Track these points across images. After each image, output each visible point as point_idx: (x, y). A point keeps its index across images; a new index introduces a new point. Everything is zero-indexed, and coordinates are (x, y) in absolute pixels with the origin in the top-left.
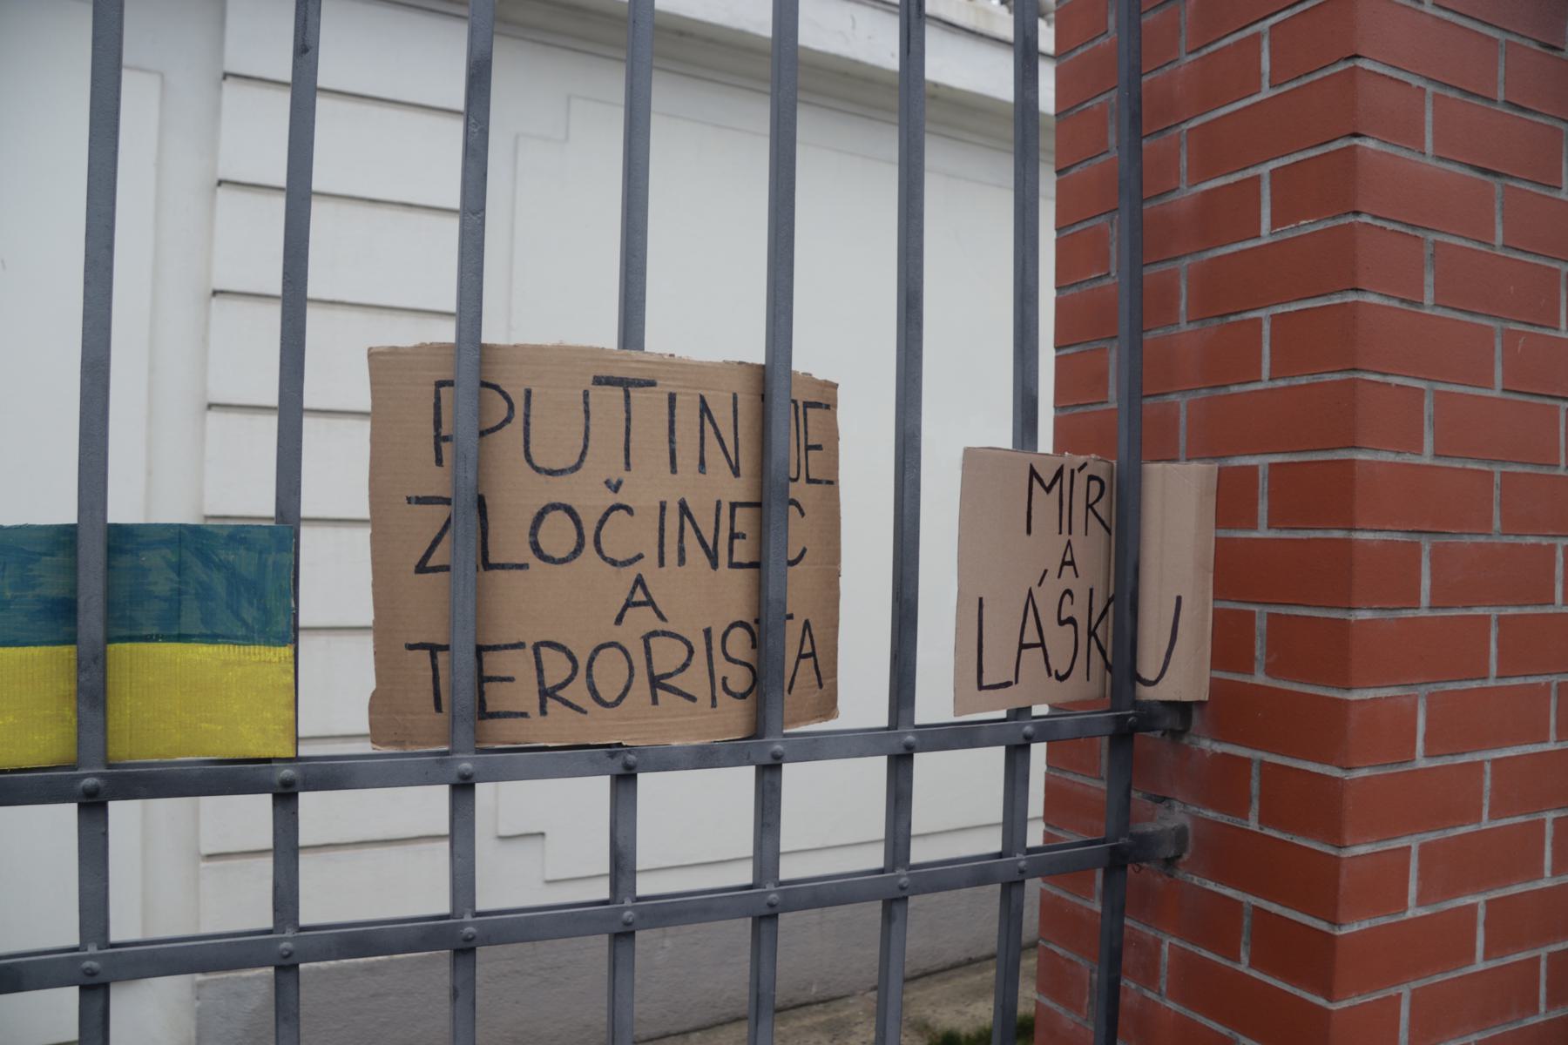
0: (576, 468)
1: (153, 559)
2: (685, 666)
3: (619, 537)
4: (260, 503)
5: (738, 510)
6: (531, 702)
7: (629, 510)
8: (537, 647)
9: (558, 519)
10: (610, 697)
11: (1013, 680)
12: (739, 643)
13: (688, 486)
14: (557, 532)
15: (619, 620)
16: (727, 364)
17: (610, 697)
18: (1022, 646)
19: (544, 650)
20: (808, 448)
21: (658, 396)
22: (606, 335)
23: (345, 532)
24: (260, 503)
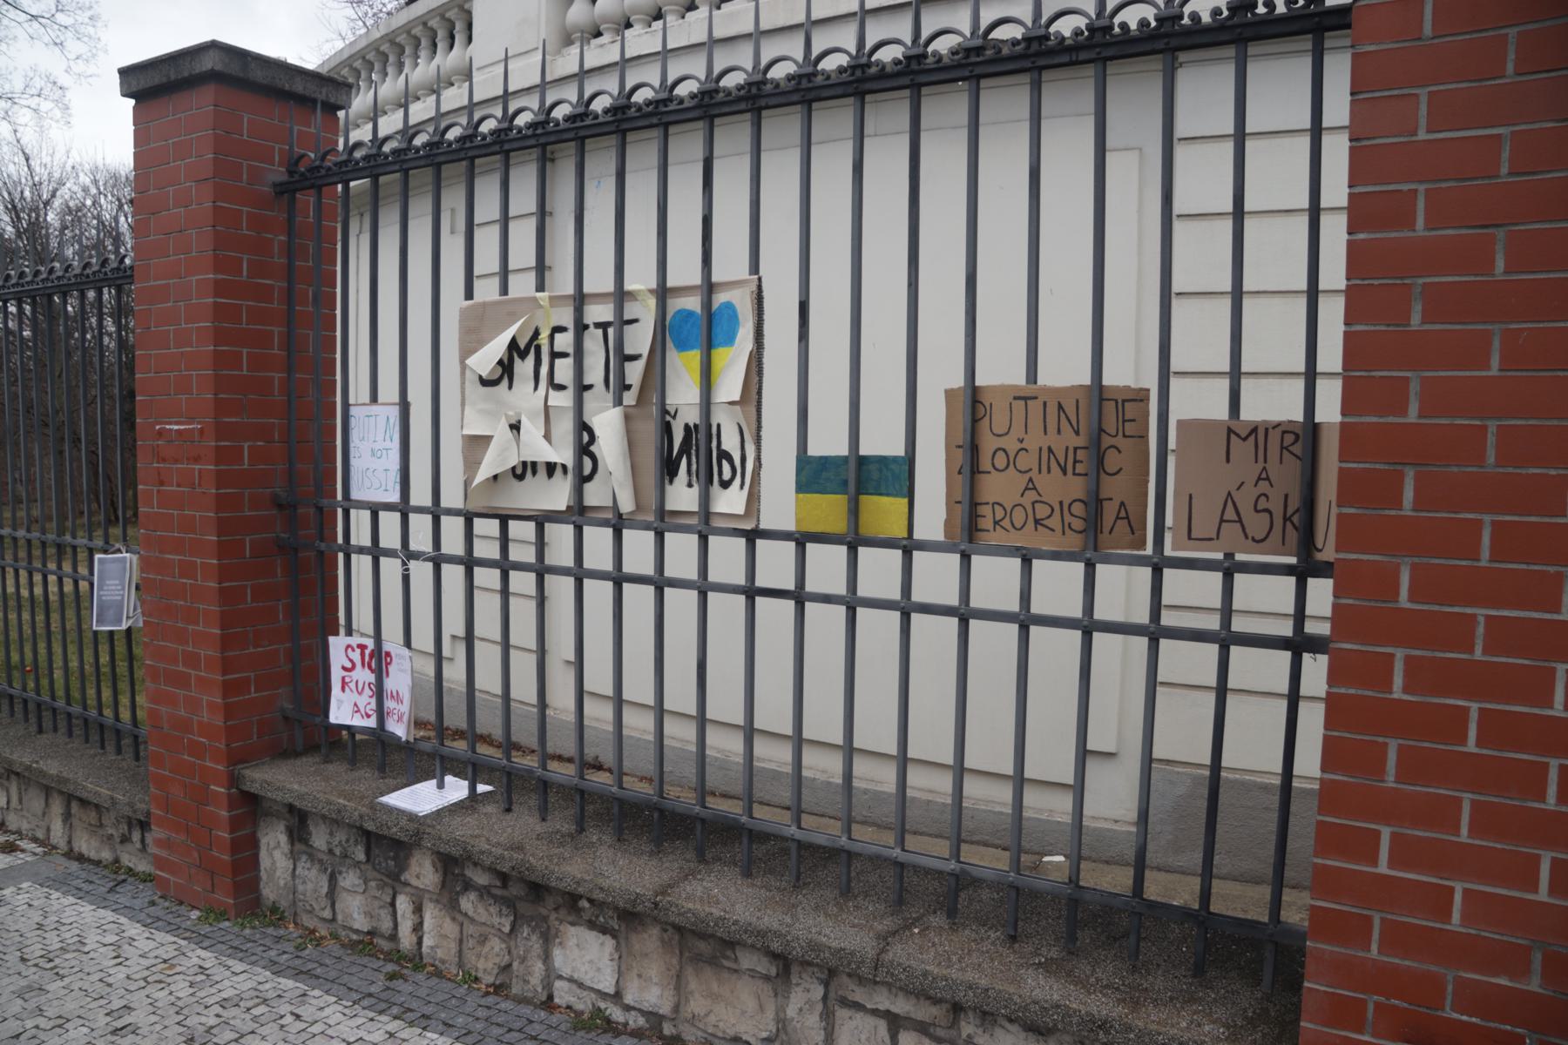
0: (1007, 434)
1: (873, 467)
2: (1050, 516)
3: (1024, 461)
4: (899, 450)
5: (1078, 451)
6: (990, 527)
7: (1026, 450)
8: (993, 504)
9: (1000, 454)
10: (1018, 526)
11: (1215, 536)
12: (1078, 509)
13: (1052, 440)
14: (1001, 461)
15: (1022, 495)
16: (1073, 387)
17: (1018, 526)
18: (1222, 521)
19: (996, 506)
20: (1124, 421)
21: (1039, 403)
22: (1020, 379)
23: (1287, 382)
24: (899, 450)
